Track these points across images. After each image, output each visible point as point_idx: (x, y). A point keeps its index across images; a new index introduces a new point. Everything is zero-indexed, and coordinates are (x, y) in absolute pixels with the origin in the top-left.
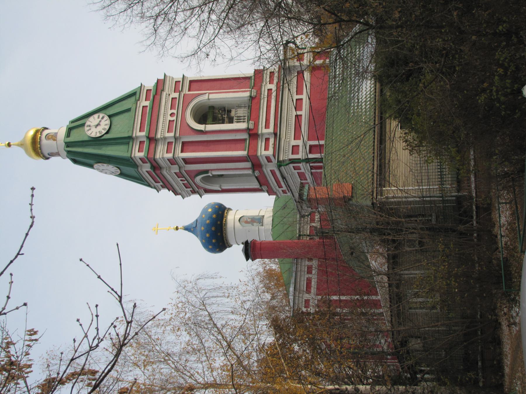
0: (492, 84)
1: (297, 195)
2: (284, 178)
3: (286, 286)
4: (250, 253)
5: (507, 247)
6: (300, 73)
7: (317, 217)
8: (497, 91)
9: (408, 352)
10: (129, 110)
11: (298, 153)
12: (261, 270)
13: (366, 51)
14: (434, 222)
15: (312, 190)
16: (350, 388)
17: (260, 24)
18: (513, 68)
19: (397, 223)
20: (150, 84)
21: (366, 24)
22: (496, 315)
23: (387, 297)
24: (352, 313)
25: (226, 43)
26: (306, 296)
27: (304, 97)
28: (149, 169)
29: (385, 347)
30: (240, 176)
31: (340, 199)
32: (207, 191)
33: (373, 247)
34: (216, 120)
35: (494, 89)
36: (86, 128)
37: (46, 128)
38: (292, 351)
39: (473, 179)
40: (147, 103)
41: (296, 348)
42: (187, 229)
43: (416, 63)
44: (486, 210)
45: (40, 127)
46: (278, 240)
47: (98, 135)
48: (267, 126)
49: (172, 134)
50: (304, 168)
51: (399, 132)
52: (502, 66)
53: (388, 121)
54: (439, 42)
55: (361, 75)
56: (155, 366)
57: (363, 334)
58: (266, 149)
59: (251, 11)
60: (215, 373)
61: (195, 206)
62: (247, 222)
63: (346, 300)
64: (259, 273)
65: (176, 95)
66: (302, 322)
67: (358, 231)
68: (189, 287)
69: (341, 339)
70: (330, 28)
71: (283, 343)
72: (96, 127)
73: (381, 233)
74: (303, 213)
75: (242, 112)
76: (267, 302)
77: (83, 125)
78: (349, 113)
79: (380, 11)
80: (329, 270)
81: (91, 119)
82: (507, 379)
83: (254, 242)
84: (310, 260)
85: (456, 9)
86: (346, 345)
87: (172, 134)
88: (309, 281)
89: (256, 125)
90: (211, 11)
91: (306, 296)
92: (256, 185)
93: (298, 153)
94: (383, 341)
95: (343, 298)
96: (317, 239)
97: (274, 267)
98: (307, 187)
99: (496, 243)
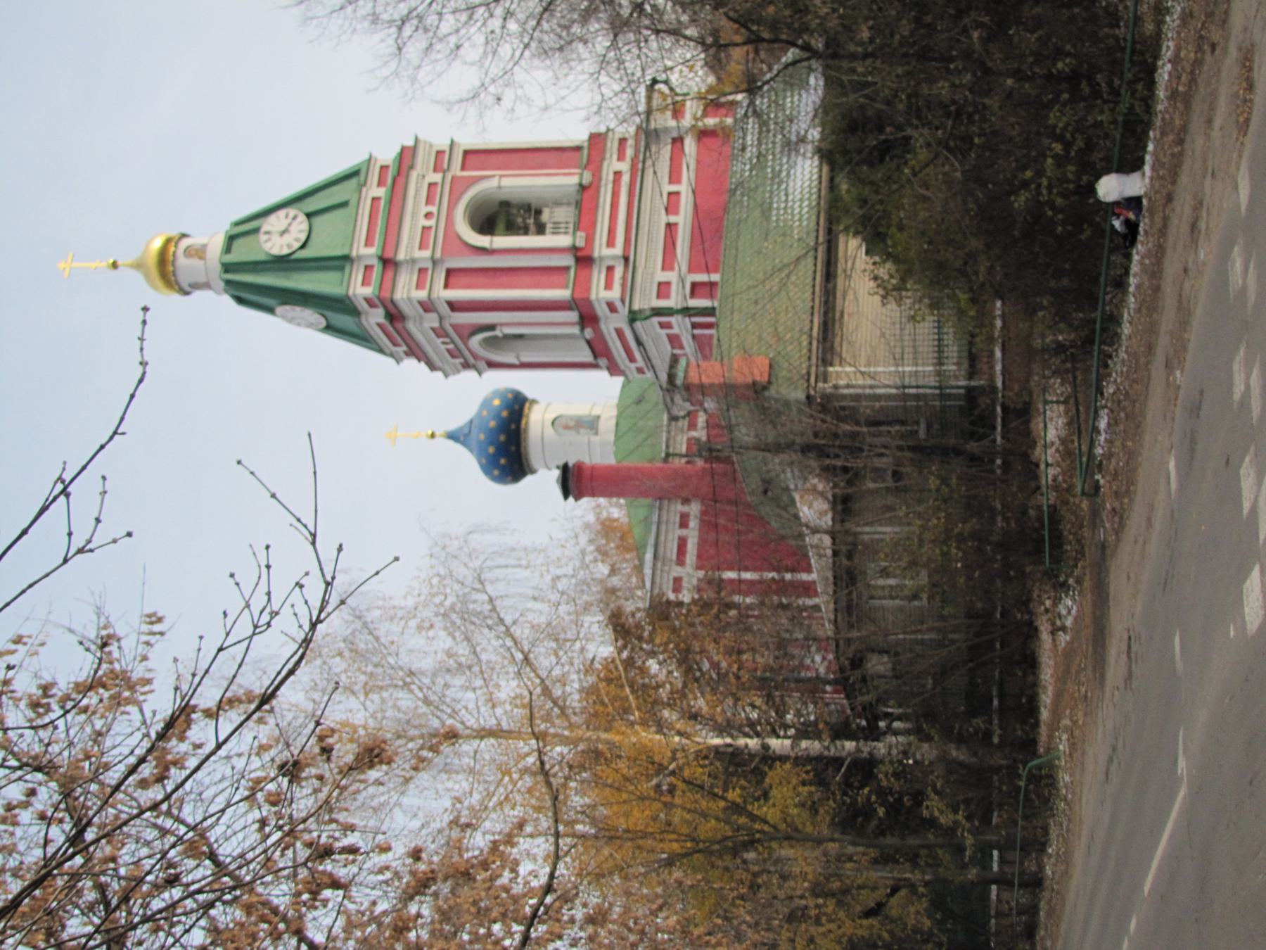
0: (1040, 173)
1: (664, 377)
2: (639, 343)
3: (639, 549)
4: (571, 484)
6: (678, 141)
7: (701, 419)
8: (1050, 188)
9: (864, 680)
10: (344, 204)
11: (667, 296)
12: (591, 518)
13: (805, 102)
14: (922, 434)
15: (692, 367)
16: (753, 743)
17: (602, 43)
18: (1080, 143)
19: (854, 436)
20: (387, 155)
21: (806, 47)
22: (1031, 613)
23: (830, 575)
24: (762, 603)
25: (536, 77)
26: (677, 571)
27: (684, 189)
28: (382, 320)
29: (822, 670)
30: (555, 337)
31: (747, 386)
32: (492, 365)
33: (805, 479)
34: (512, 228)
35: (1045, 182)
36: (263, 237)
37: (184, 236)
38: (643, 671)
39: (998, 354)
41: (653, 665)
42: (452, 436)
43: (900, 128)
45: (174, 233)
46: (626, 463)
47: (285, 251)
48: (611, 243)
50: (680, 325)
52: (1060, 138)
53: (842, 239)
54: (942, 89)
55: (791, 147)
56: (385, 694)
57: (782, 645)
58: (608, 286)
60: (499, 711)
61: (471, 393)
62: (566, 427)
63: (751, 582)
64: (587, 526)
65: (437, 178)
66: (667, 618)
67: (777, 448)
69: (740, 652)
72: (282, 236)
73: (821, 452)
74: (676, 412)
75: (564, 214)
76: (602, 581)
77: (256, 231)
78: (768, 219)
80: (722, 521)
81: (272, 218)
82: (1043, 730)
83: (579, 467)
84: (686, 501)
85: (979, 25)
86: (749, 665)
87: (427, 254)
88: (682, 543)
89: (590, 239)
91: (677, 571)
92: (587, 356)
93: (667, 296)
94: (818, 658)
95: (747, 576)
96: (700, 463)
97: (616, 513)
98: (683, 362)
99: (1036, 477)
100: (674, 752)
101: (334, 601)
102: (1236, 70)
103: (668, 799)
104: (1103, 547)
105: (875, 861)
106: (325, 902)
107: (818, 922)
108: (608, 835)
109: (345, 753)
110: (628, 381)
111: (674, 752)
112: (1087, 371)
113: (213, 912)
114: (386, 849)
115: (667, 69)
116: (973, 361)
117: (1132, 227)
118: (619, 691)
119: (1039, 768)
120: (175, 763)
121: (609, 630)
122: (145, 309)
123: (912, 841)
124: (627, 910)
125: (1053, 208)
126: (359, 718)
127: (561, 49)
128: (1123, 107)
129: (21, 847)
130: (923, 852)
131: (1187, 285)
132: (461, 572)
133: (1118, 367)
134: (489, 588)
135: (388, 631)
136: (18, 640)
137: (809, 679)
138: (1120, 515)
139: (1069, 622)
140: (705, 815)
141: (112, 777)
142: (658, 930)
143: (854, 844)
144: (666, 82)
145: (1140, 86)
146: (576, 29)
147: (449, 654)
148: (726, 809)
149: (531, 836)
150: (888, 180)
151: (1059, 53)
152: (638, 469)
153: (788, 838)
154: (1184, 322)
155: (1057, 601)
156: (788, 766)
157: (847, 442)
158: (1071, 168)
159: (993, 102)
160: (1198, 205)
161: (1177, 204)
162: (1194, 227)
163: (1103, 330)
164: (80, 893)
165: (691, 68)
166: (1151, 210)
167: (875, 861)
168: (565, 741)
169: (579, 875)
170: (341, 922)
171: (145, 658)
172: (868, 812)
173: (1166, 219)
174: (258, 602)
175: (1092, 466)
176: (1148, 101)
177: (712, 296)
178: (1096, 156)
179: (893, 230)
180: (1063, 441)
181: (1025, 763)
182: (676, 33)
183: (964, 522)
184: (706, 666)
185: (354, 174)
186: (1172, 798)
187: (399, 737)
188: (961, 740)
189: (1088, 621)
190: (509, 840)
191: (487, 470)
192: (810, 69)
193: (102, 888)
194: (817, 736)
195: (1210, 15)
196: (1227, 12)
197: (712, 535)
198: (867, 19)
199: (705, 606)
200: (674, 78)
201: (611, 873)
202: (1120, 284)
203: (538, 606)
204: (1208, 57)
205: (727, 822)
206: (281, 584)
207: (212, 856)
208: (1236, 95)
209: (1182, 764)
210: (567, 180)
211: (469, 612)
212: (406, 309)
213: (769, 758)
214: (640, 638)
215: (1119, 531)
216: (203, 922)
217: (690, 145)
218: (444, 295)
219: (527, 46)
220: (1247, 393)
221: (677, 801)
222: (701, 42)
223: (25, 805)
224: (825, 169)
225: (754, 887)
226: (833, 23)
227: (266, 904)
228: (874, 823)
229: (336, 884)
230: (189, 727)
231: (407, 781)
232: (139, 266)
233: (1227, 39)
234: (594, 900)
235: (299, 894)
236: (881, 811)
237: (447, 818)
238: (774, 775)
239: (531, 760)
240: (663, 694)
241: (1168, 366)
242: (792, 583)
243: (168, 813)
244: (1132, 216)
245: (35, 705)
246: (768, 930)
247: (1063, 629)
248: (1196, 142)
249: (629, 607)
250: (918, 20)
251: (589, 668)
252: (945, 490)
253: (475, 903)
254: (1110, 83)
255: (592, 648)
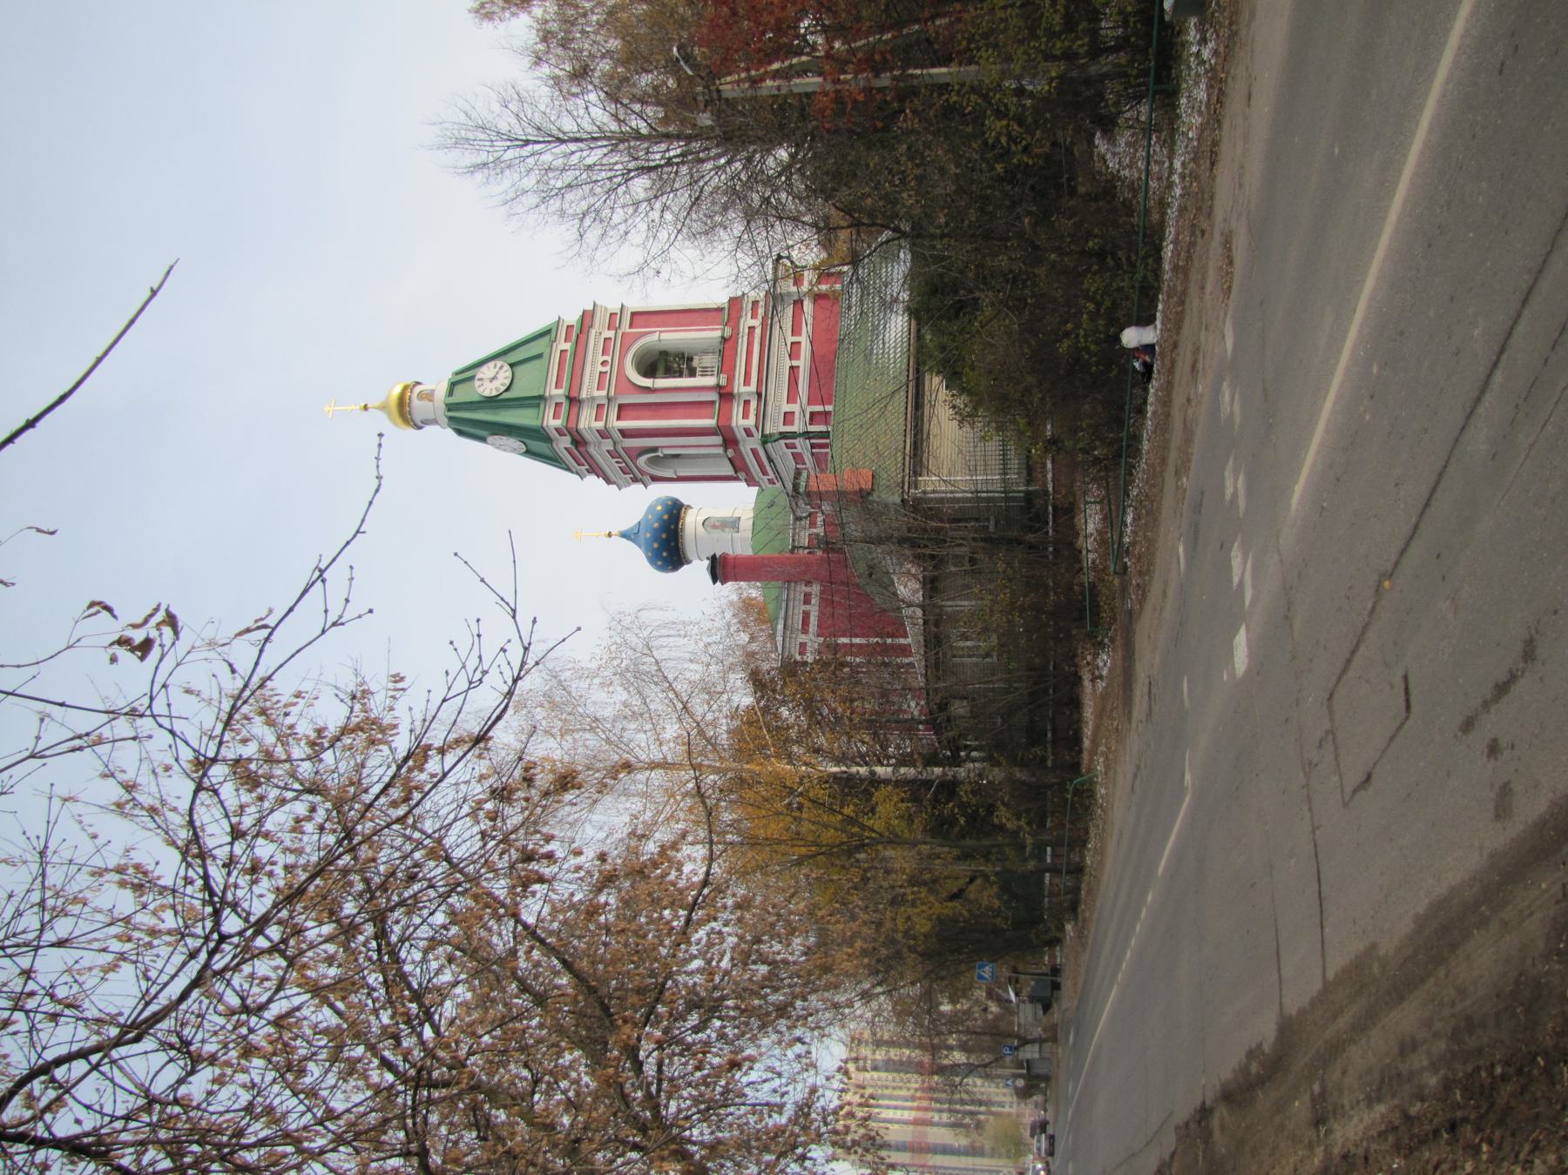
0: (1078, 326)
1: (790, 486)
2: (770, 460)
3: (772, 622)
4: (719, 572)
5: (1094, 568)
6: (798, 303)
7: (820, 518)
8: (1086, 337)
9: (949, 720)
10: (539, 356)
11: (792, 423)
12: (734, 597)
13: (897, 272)
14: (992, 529)
15: (812, 478)
16: (863, 770)
17: (738, 228)
18: (1107, 303)
19: (938, 530)
20: (572, 318)
21: (896, 230)
22: (1076, 666)
23: (921, 639)
24: (869, 662)
25: (687, 255)
26: (802, 638)
27: (804, 339)
28: (569, 445)
29: (916, 713)
30: (705, 456)
31: (855, 493)
32: (655, 479)
33: (902, 565)
34: (670, 372)
35: (1082, 332)
36: (477, 383)
38: (777, 717)
39: (1049, 466)
40: (568, 346)
41: (784, 712)
42: (624, 535)
43: (970, 291)
44: (1068, 512)
45: (409, 382)
46: (761, 554)
47: (494, 393)
48: (747, 382)
49: (604, 393)
50: (802, 445)
51: (943, 394)
52: (1092, 299)
53: (927, 377)
54: (1002, 261)
55: (887, 305)
56: (576, 736)
57: (885, 694)
58: (745, 416)
59: (725, 208)
60: (665, 748)
61: (639, 502)
62: (714, 527)
63: (860, 645)
64: (731, 603)
65: (611, 334)
66: (795, 675)
67: (879, 541)
68: (627, 621)
69: (852, 701)
70: (843, 235)
71: (766, 706)
72: (492, 382)
73: (914, 544)
74: (799, 514)
75: (710, 361)
76: (744, 647)
77: (472, 378)
78: (869, 363)
79: (917, 211)
80: (836, 599)
81: (484, 369)
82: (1085, 755)
83: (724, 557)
84: (809, 583)
85: (1029, 213)
86: (859, 710)
88: (806, 615)
89: (731, 379)
90: (665, 208)
91: (802, 638)
92: (729, 471)
93: (792, 423)
94: (913, 704)
95: (857, 641)
96: (819, 553)
97: (754, 593)
98: (804, 474)
99: (1080, 561)
100: (802, 778)
101: (530, 662)
102: (1220, 250)
103: (797, 814)
104: (1130, 613)
105: (958, 858)
106: (534, 894)
107: (914, 905)
108: (753, 842)
109: (543, 780)
110: (762, 490)
111: (802, 778)
112: (1116, 477)
113: (450, 900)
114: (578, 853)
115: (788, 247)
116: (1030, 470)
117: (1148, 368)
118: (756, 732)
119: (1082, 784)
120: (416, 788)
121: (750, 685)
122: (381, 435)
123: (986, 842)
124: (766, 898)
125: (1088, 351)
126: (557, 755)
127: (706, 233)
128: (1139, 276)
129: (308, 850)
130: (995, 850)
131: (1190, 412)
132: (633, 640)
133: (1140, 474)
134: (655, 653)
135: (577, 687)
136: (298, 695)
137: (906, 721)
138: (1143, 589)
139: (1105, 673)
140: (826, 826)
141: (367, 798)
142: (791, 913)
143: (942, 846)
144: (788, 258)
145: (1150, 261)
146: (718, 218)
147: (625, 704)
148: (842, 821)
149: (692, 844)
150: (962, 331)
151: (1089, 235)
152: (770, 559)
153: (890, 842)
154: (1188, 441)
155: (1096, 655)
156: (890, 788)
157: (933, 535)
158: (1101, 322)
159: (1040, 271)
160: (1196, 351)
161: (1181, 350)
162: (1194, 367)
163: (1128, 446)
164: (351, 884)
165: (807, 246)
166: (1161, 353)
167: (958, 858)
168: (716, 771)
169: (729, 872)
170: (547, 909)
171: (392, 709)
172: (953, 821)
173: (1173, 362)
174: (472, 663)
175: (1123, 551)
176: (1157, 272)
177: (826, 423)
178: (1120, 313)
179: (967, 369)
180: (1100, 532)
181: (1071, 781)
182: (795, 219)
183: (1025, 596)
184: (826, 711)
185: (547, 332)
186: (1180, 802)
187: (589, 769)
188: (1023, 765)
189: (1119, 671)
190: (674, 846)
191: (652, 561)
192: (900, 247)
193: (367, 881)
194: (913, 764)
195: (1199, 209)
196: (1211, 207)
197: (829, 609)
198: (942, 209)
199: (823, 664)
200: (794, 254)
201: (754, 871)
202: (1141, 411)
203: (693, 666)
204: (1199, 240)
205: (843, 831)
206: (489, 650)
207: (448, 859)
208: (1221, 268)
209: (1188, 777)
210: (712, 334)
211: (640, 671)
212: (588, 436)
213: (875, 782)
214: (774, 691)
215: (1142, 601)
216: (443, 908)
217: (808, 305)
218: (617, 425)
219: (679, 231)
220: (1235, 494)
221: (804, 816)
222: (815, 225)
223: (309, 819)
224: (913, 323)
225: (865, 880)
226: (917, 211)
227: (490, 894)
228: (957, 829)
229: (541, 879)
230: (426, 761)
231: (595, 802)
232: (383, 408)
233: (1212, 226)
234: (741, 892)
235: (514, 887)
236: (962, 821)
237: (627, 830)
238: (879, 795)
239: (691, 785)
240: (793, 733)
241: (1177, 473)
242: (892, 646)
243: (414, 827)
244: (1148, 359)
245: (312, 744)
246: (875, 911)
247: (1101, 677)
248: (1193, 303)
249: (765, 666)
250: (982, 210)
251: (733, 716)
252: (1010, 572)
253: (650, 894)
254: (1128, 258)
255: (736, 699)
